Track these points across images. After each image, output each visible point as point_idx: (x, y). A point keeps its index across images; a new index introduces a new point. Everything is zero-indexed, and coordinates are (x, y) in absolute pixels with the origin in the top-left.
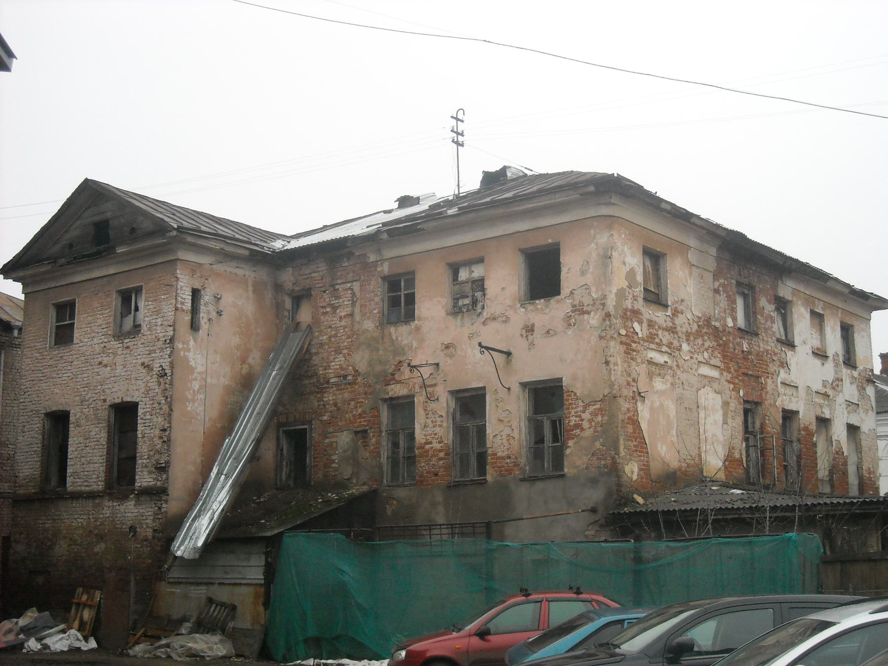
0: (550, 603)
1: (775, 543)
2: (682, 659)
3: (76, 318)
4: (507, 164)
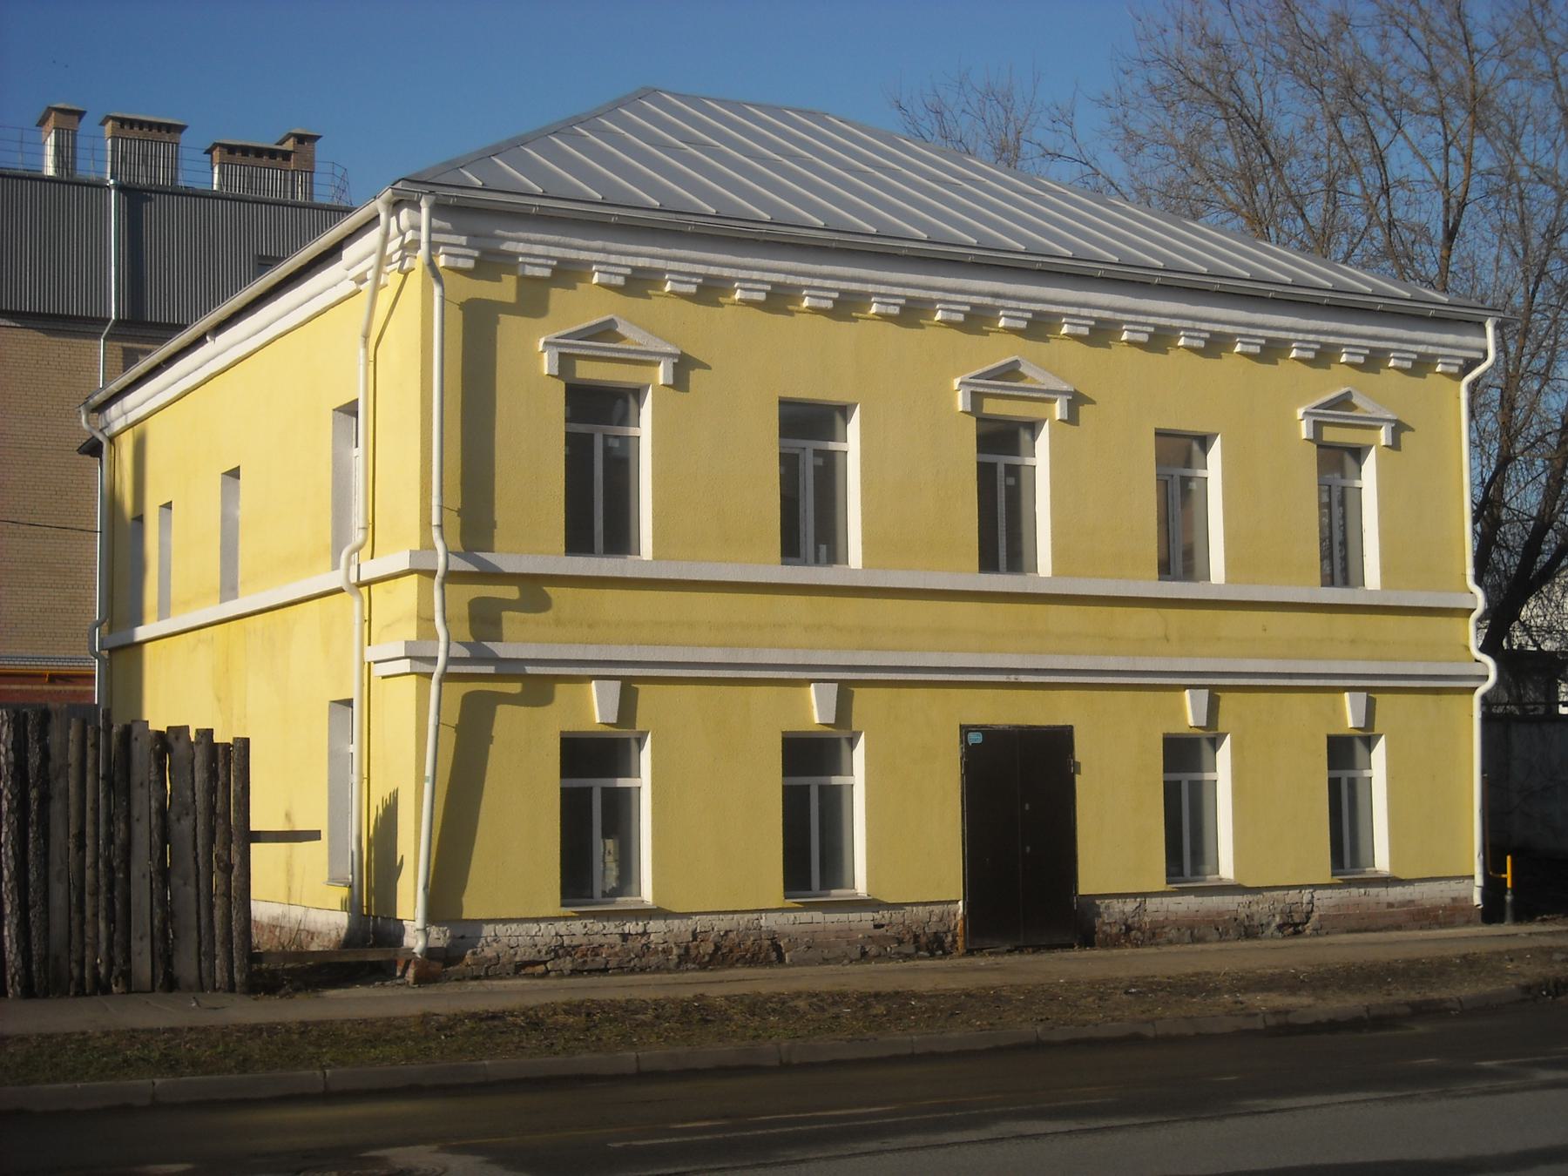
0: (373, 586)
1: (577, 915)
2: (141, 633)
3: (1069, 724)
4: (1211, 363)
